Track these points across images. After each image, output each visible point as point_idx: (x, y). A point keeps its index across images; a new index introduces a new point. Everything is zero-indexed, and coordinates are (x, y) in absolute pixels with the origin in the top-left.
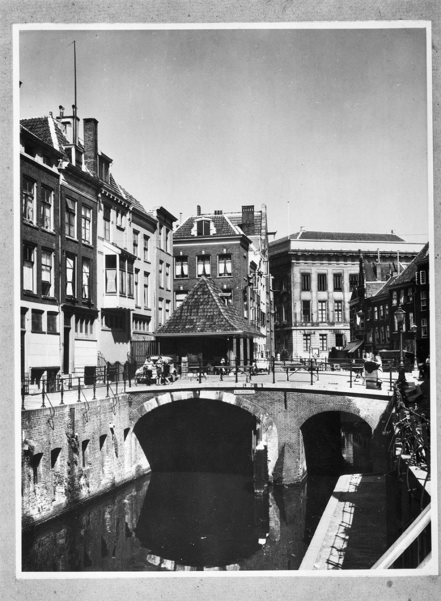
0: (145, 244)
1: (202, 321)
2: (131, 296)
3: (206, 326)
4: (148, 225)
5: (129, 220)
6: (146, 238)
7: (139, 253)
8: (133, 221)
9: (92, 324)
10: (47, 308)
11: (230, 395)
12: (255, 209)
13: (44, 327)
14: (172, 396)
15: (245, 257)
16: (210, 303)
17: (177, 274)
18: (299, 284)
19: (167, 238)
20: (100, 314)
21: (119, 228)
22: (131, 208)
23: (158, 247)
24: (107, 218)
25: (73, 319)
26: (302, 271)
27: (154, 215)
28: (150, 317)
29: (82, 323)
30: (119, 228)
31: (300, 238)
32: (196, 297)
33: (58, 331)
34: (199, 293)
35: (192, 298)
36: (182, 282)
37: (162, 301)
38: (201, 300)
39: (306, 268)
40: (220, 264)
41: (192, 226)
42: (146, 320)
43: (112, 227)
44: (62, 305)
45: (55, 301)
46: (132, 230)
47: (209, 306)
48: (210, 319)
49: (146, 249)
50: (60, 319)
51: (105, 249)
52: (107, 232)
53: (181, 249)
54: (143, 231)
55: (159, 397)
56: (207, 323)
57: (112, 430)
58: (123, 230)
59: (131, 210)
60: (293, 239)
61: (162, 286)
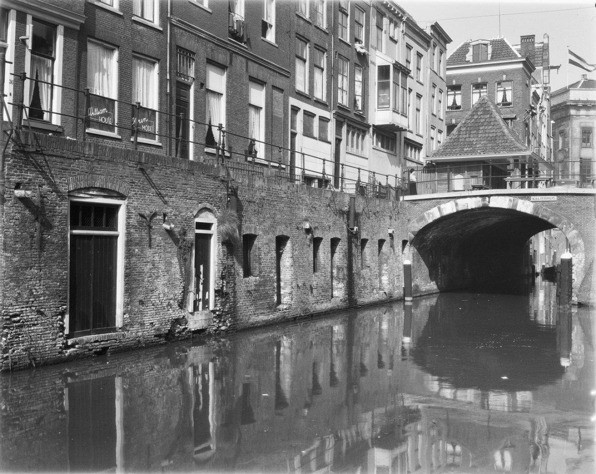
0: (418, 63)
1: (482, 142)
2: (404, 115)
3: (488, 148)
4: (421, 42)
5: (403, 31)
6: (419, 55)
7: (412, 67)
8: (406, 34)
9: (363, 138)
10: (319, 112)
11: (527, 202)
12: (537, 40)
13: (316, 133)
14: (457, 204)
15: (527, 85)
16: (492, 124)
17: (448, 105)
18: (578, 140)
19: (440, 61)
20: (371, 129)
21: (392, 39)
22: (404, 19)
23: (432, 68)
24: (379, 27)
25: (344, 129)
26: (583, 125)
27: (429, 31)
28: (422, 145)
29: (353, 135)
30: (392, 39)
31: (580, 88)
32: (476, 117)
33: (329, 140)
34: (479, 113)
35: (471, 119)
36: (455, 114)
37: (434, 129)
38: (482, 121)
39: (588, 121)
40: (498, 93)
41: (467, 51)
42: (417, 147)
43: (384, 38)
44: (334, 112)
45: (327, 106)
46: (405, 44)
47: (491, 127)
48: (494, 140)
49: (418, 69)
50: (331, 126)
51: (379, 58)
52: (380, 41)
53: (454, 77)
54: (416, 48)
55: (442, 206)
56: (488, 145)
57: (391, 235)
58: (396, 42)
59: (405, 20)
60: (572, 89)
61: (435, 113)
